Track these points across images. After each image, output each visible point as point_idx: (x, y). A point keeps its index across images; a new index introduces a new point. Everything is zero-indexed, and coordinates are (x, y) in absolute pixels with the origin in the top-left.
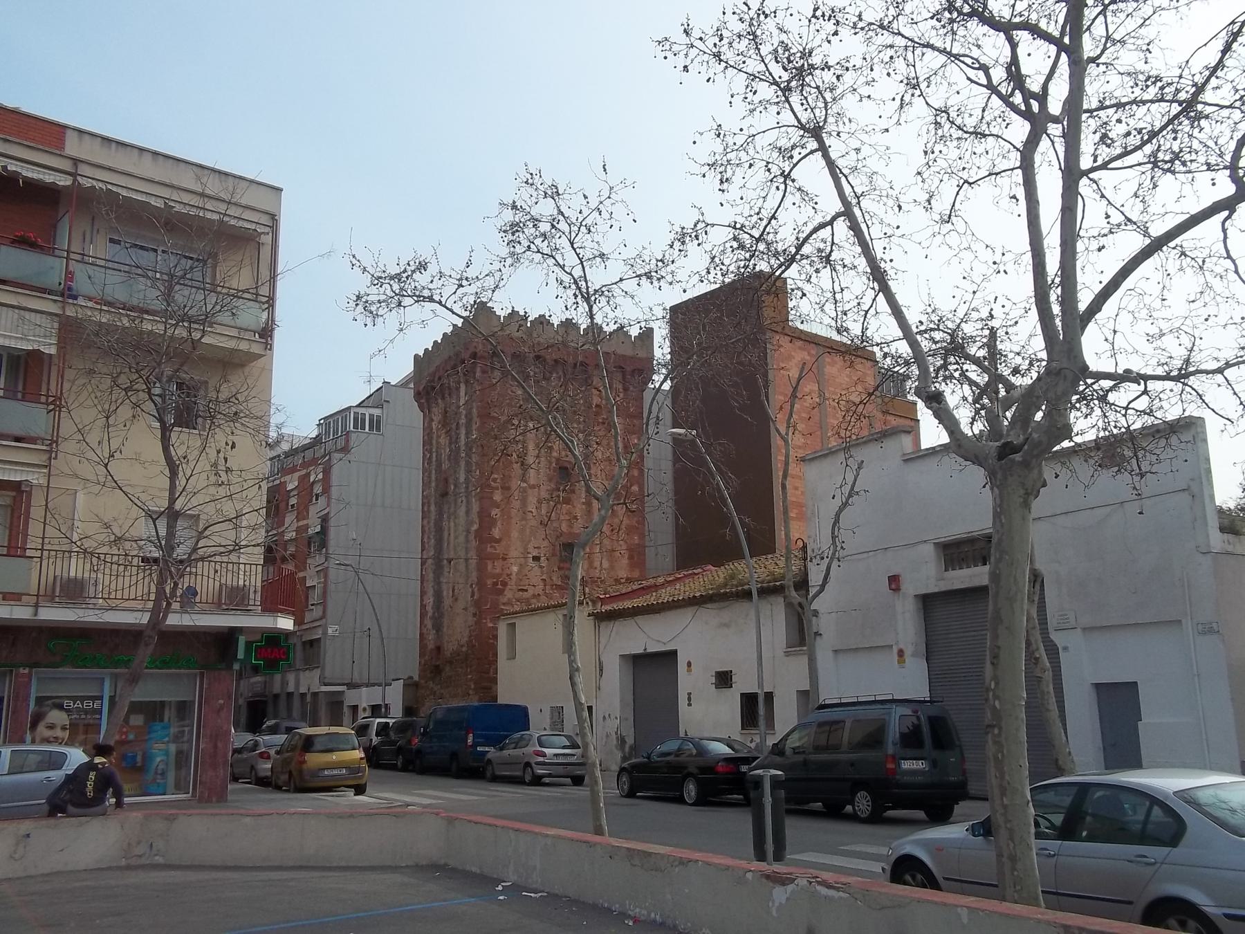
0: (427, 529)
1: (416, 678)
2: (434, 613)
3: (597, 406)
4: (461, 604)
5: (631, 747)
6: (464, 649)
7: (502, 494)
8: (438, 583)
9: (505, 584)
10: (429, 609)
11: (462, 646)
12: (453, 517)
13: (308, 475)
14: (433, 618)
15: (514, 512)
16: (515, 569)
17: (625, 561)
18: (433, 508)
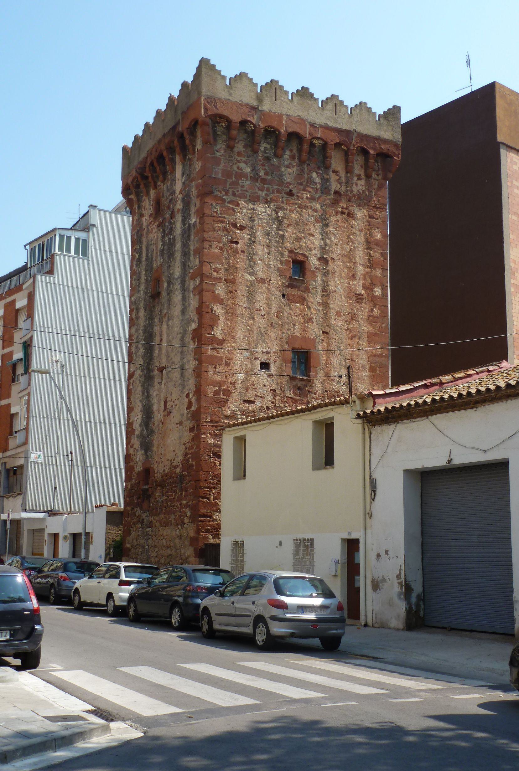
0: (134, 338)
1: (121, 506)
2: (142, 431)
3: (336, 192)
4: (175, 417)
5: (418, 596)
6: (178, 470)
8: (147, 395)
9: (228, 393)
10: (137, 426)
11: (175, 467)
12: (165, 320)
13: (14, 302)
14: (141, 436)
15: (239, 310)
16: (241, 376)
17: (365, 374)
18: (142, 313)
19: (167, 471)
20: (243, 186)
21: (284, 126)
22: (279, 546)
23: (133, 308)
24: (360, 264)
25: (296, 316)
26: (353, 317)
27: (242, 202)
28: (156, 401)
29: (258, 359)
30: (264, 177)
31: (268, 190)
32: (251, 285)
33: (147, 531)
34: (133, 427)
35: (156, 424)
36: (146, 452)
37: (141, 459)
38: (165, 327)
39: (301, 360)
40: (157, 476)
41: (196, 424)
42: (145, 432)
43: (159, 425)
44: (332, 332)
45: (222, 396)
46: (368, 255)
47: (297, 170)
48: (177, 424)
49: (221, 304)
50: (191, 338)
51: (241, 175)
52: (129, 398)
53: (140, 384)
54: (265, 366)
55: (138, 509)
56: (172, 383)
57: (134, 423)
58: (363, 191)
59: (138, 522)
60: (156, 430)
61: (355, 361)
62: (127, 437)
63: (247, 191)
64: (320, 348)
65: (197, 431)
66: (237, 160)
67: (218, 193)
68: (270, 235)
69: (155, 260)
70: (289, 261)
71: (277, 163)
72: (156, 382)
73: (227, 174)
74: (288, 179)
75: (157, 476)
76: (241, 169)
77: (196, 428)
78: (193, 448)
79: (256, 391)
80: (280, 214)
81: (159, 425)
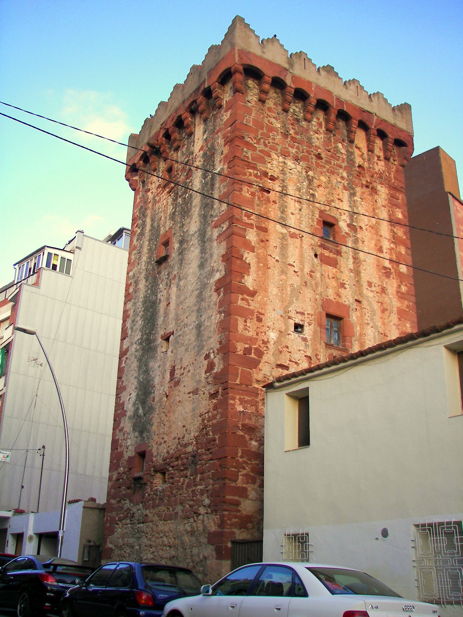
3: (359, 166)
6: (190, 449)
7: (258, 235)
9: (260, 354)
10: (129, 408)
11: (186, 446)
15: (271, 262)
19: (171, 452)
20: (274, 139)
21: (314, 92)
22: (380, 537)
23: (131, 283)
24: (386, 238)
25: (329, 278)
26: (383, 290)
27: (274, 156)
28: (158, 373)
29: (292, 319)
30: (293, 135)
31: (298, 148)
32: (283, 237)
33: (139, 527)
34: (124, 408)
35: (157, 399)
36: (141, 433)
37: (133, 442)
38: (174, 289)
39: (335, 329)
40: (157, 460)
41: (220, 388)
42: (141, 411)
43: (161, 399)
44: (364, 302)
45: (253, 356)
46: (392, 231)
47: (324, 137)
48: (189, 393)
49: (253, 251)
50: (213, 291)
51: (271, 129)
52: (119, 378)
53: (135, 360)
54: (298, 327)
55: (127, 501)
56: (183, 349)
57: (126, 403)
58: (384, 171)
59: (125, 517)
60: (157, 407)
61: (387, 336)
62: (115, 420)
63: (277, 144)
64: (354, 317)
65: (222, 396)
66: (267, 114)
67: (249, 139)
68: (302, 191)
69: (163, 226)
70: (320, 221)
71: (305, 126)
72: (158, 352)
73: (259, 125)
74: (316, 143)
75: (157, 460)
76: (271, 123)
77: (220, 393)
78: (215, 418)
79: (290, 355)
80: (310, 173)
81: (161, 399)
